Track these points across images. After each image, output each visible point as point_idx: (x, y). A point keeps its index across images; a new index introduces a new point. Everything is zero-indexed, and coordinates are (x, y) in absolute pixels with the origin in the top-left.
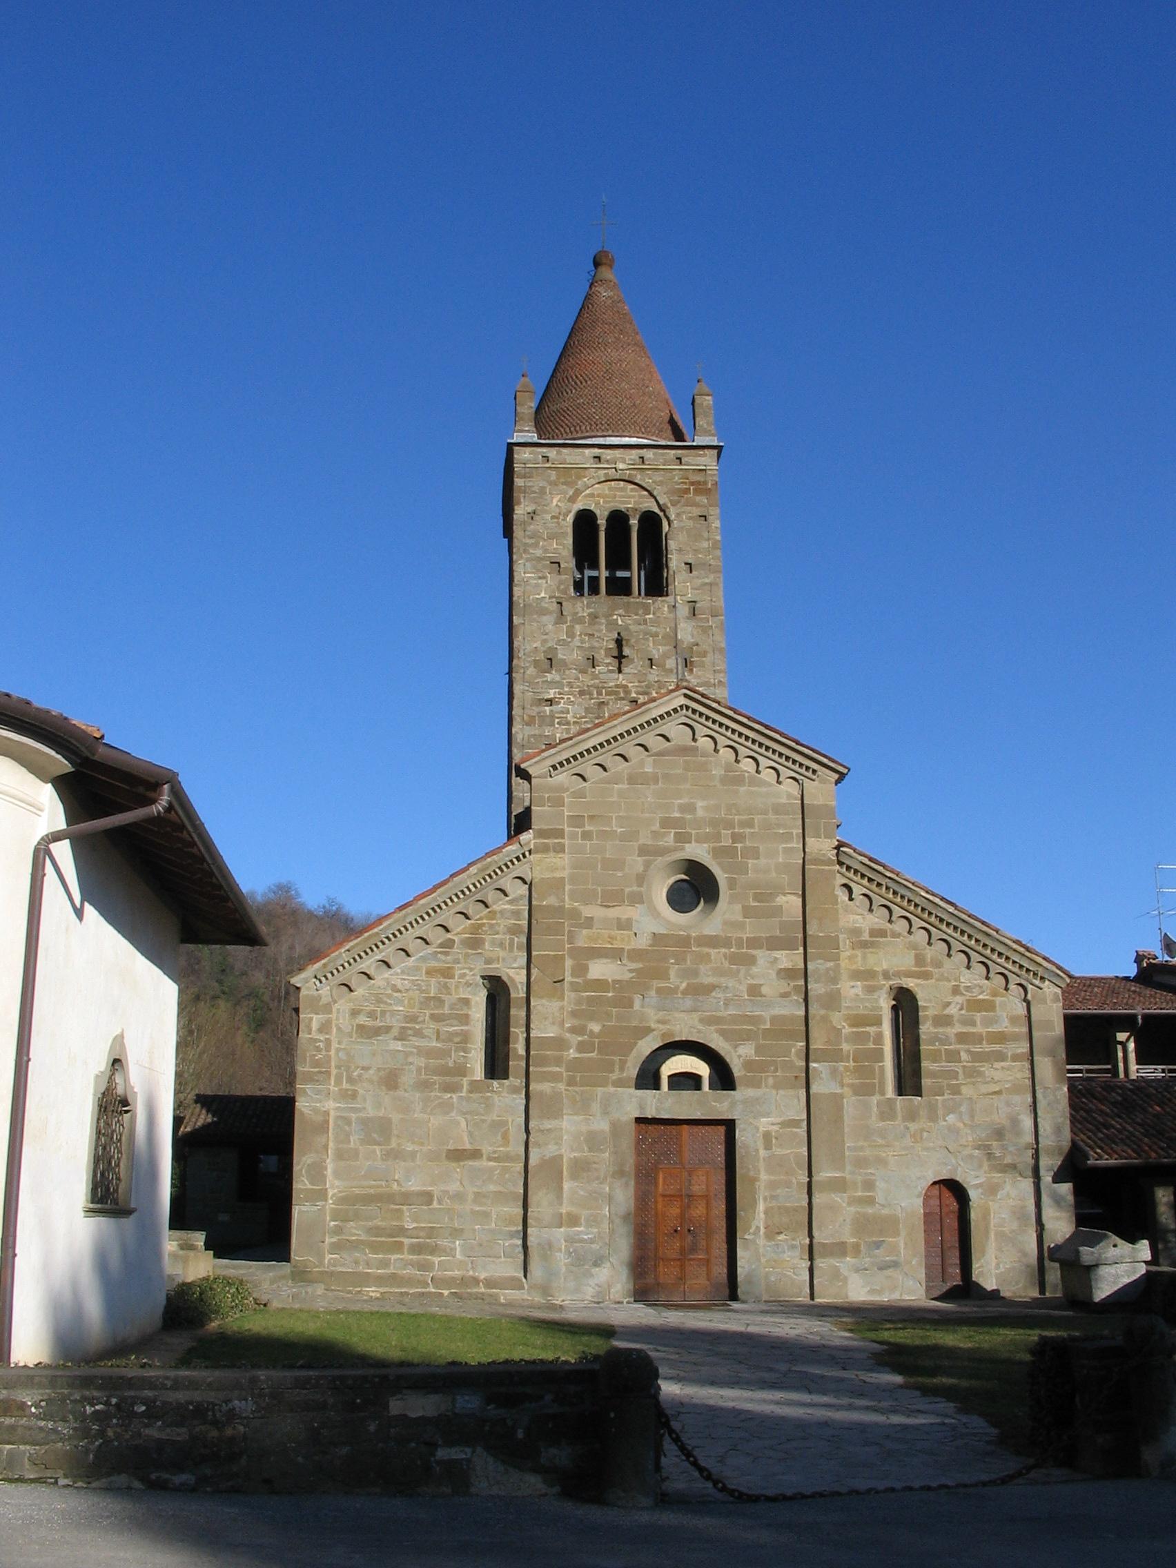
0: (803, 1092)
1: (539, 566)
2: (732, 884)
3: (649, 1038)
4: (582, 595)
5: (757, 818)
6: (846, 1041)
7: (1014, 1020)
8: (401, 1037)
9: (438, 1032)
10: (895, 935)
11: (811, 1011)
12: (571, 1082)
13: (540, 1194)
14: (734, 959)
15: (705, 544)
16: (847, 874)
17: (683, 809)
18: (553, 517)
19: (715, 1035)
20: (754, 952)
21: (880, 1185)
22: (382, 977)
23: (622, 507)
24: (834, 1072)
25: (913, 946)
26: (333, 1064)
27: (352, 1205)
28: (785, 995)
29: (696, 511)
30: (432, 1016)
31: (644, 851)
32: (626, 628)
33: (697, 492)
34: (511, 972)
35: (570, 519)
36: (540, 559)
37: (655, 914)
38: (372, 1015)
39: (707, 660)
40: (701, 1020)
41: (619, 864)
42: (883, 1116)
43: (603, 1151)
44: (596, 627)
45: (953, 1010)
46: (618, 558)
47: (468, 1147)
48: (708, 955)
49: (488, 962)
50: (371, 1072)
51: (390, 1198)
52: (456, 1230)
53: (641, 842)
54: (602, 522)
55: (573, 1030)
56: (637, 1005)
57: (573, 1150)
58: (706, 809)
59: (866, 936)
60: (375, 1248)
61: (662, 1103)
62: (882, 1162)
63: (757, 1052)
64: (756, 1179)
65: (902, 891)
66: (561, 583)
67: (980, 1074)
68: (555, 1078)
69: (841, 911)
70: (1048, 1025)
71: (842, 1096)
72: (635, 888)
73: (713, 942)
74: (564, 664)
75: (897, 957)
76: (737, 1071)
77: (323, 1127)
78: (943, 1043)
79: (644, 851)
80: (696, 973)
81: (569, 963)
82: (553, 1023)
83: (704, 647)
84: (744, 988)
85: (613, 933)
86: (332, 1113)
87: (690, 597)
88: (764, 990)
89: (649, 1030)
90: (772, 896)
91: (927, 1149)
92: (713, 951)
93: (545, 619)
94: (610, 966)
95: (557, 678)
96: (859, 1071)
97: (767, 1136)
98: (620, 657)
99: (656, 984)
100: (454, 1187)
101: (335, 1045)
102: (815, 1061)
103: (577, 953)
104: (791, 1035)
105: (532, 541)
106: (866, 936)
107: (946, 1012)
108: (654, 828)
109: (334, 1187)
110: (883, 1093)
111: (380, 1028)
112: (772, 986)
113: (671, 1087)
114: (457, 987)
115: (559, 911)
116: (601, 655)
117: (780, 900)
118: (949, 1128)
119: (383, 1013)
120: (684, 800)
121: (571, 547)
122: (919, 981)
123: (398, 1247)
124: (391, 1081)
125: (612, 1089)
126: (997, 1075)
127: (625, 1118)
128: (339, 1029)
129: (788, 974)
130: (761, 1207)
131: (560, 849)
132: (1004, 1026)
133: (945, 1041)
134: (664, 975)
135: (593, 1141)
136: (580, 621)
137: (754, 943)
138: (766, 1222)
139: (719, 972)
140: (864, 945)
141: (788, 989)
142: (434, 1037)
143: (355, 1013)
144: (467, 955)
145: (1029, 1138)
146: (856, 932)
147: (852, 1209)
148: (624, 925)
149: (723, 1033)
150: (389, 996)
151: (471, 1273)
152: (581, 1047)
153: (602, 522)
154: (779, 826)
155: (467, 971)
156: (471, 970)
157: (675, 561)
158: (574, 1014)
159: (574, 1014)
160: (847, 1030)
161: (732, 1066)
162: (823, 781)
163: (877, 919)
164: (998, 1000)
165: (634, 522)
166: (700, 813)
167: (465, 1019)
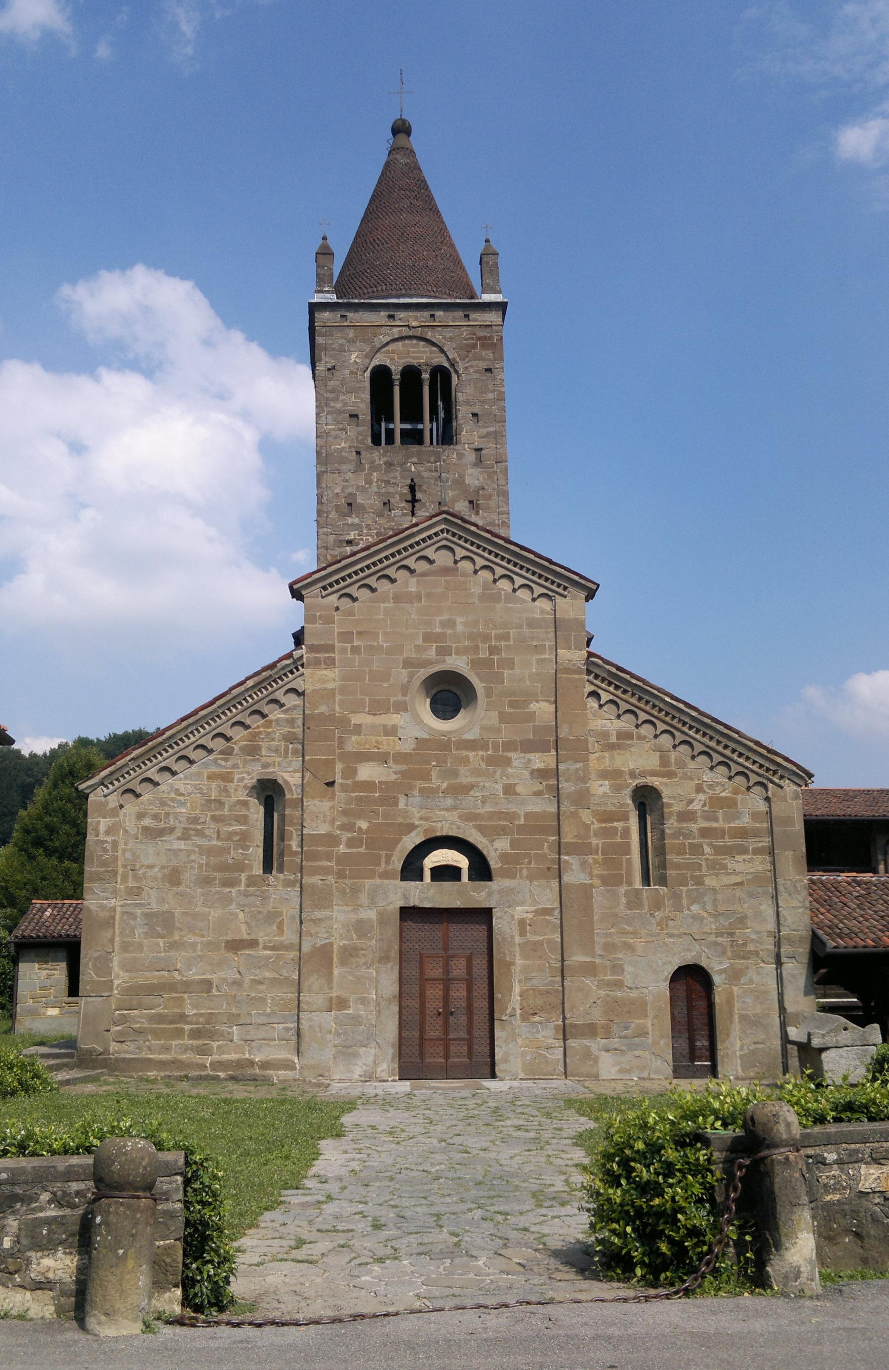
0: (555, 884)
1: (340, 418)
2: (489, 693)
3: (413, 834)
4: (380, 444)
5: (512, 632)
6: (595, 835)
7: (755, 816)
8: (185, 837)
9: (218, 832)
10: (641, 738)
11: (562, 808)
12: (341, 875)
13: (311, 979)
14: (491, 761)
15: (491, 396)
16: (595, 681)
17: (443, 624)
18: (352, 373)
19: (474, 831)
20: (510, 754)
21: (628, 968)
22: (167, 783)
23: (415, 362)
24: (583, 864)
25: (658, 749)
26: (119, 864)
27: (138, 993)
28: (538, 794)
29: (484, 365)
30: (213, 818)
31: (407, 664)
32: (419, 474)
33: (483, 346)
34: (286, 776)
35: (367, 374)
36: (340, 412)
37: (419, 721)
38: (156, 817)
39: (492, 503)
40: (460, 817)
41: (386, 676)
42: (629, 906)
43: (371, 939)
44: (392, 475)
45: (696, 806)
46: (412, 412)
47: (246, 937)
48: (467, 757)
49: (265, 766)
50: (156, 870)
51: (171, 987)
52: (233, 1015)
53: (405, 656)
54: (396, 377)
55: (342, 827)
56: (402, 804)
57: (342, 938)
58: (465, 624)
59: (613, 739)
60: (157, 1035)
61: (425, 893)
62: (630, 948)
63: (512, 847)
64: (513, 964)
65: (732, 745)
66: (359, 433)
67: (725, 867)
68: (326, 871)
69: (590, 716)
70: (789, 821)
71: (592, 886)
72: (400, 698)
73: (472, 745)
74: (362, 507)
75: (642, 758)
76: (494, 864)
77: (109, 922)
78: (686, 836)
79: (407, 664)
80: (456, 774)
81: (339, 766)
82: (324, 822)
83: (490, 491)
84: (499, 787)
85: (379, 738)
86: (119, 909)
87: (476, 445)
88: (519, 789)
89: (411, 827)
90: (526, 703)
91: (671, 936)
92: (471, 754)
93: (344, 467)
94: (377, 768)
95: (356, 521)
96: (607, 863)
97: (522, 923)
98: (413, 501)
99: (419, 784)
100: (231, 975)
101: (122, 846)
102: (568, 854)
103: (344, 757)
104: (542, 830)
105: (334, 395)
106: (613, 739)
107: (690, 807)
108: (417, 643)
109: (120, 978)
110: (630, 883)
111: (164, 829)
112: (526, 786)
113: (433, 878)
114: (236, 790)
115: (330, 718)
116: (396, 500)
117: (534, 707)
118: (694, 917)
119: (167, 814)
120: (445, 617)
121: (369, 400)
122: (664, 780)
123: (179, 1033)
124: (174, 878)
125: (378, 881)
126: (740, 867)
127: (390, 908)
128: (126, 831)
129: (542, 774)
130: (517, 989)
131: (330, 663)
132: (745, 821)
133: (689, 835)
134: (426, 777)
135: (361, 928)
136: (377, 468)
137: (509, 746)
138: (521, 1004)
139: (477, 772)
140: (612, 747)
141: (541, 788)
142: (215, 836)
143: (140, 816)
144: (245, 761)
145: (771, 926)
146: (605, 734)
147: (602, 993)
148: (391, 731)
149: (480, 829)
150: (173, 800)
151: (247, 1056)
152: (350, 843)
153: (396, 377)
154: (532, 638)
155: (245, 775)
156: (249, 773)
157: (463, 412)
158: (345, 813)
159: (345, 813)
160: (596, 826)
161: (489, 859)
162: (574, 598)
163: (626, 723)
164: (739, 797)
165: (426, 376)
166: (460, 628)
167: (243, 820)
